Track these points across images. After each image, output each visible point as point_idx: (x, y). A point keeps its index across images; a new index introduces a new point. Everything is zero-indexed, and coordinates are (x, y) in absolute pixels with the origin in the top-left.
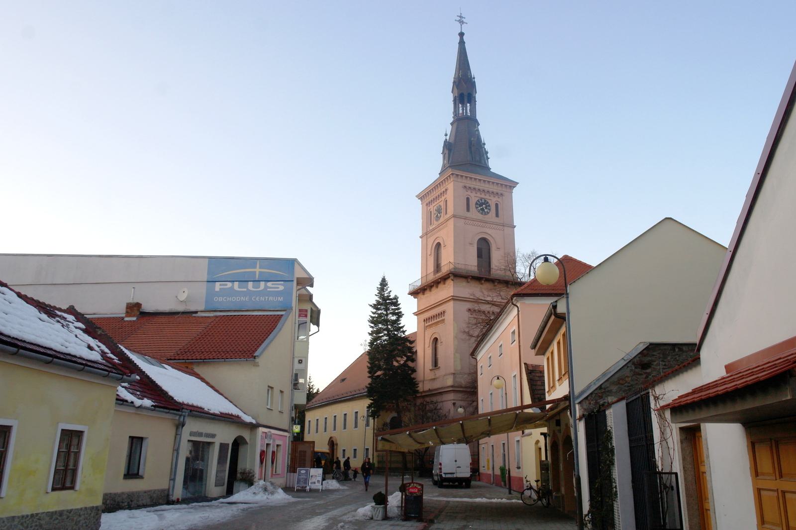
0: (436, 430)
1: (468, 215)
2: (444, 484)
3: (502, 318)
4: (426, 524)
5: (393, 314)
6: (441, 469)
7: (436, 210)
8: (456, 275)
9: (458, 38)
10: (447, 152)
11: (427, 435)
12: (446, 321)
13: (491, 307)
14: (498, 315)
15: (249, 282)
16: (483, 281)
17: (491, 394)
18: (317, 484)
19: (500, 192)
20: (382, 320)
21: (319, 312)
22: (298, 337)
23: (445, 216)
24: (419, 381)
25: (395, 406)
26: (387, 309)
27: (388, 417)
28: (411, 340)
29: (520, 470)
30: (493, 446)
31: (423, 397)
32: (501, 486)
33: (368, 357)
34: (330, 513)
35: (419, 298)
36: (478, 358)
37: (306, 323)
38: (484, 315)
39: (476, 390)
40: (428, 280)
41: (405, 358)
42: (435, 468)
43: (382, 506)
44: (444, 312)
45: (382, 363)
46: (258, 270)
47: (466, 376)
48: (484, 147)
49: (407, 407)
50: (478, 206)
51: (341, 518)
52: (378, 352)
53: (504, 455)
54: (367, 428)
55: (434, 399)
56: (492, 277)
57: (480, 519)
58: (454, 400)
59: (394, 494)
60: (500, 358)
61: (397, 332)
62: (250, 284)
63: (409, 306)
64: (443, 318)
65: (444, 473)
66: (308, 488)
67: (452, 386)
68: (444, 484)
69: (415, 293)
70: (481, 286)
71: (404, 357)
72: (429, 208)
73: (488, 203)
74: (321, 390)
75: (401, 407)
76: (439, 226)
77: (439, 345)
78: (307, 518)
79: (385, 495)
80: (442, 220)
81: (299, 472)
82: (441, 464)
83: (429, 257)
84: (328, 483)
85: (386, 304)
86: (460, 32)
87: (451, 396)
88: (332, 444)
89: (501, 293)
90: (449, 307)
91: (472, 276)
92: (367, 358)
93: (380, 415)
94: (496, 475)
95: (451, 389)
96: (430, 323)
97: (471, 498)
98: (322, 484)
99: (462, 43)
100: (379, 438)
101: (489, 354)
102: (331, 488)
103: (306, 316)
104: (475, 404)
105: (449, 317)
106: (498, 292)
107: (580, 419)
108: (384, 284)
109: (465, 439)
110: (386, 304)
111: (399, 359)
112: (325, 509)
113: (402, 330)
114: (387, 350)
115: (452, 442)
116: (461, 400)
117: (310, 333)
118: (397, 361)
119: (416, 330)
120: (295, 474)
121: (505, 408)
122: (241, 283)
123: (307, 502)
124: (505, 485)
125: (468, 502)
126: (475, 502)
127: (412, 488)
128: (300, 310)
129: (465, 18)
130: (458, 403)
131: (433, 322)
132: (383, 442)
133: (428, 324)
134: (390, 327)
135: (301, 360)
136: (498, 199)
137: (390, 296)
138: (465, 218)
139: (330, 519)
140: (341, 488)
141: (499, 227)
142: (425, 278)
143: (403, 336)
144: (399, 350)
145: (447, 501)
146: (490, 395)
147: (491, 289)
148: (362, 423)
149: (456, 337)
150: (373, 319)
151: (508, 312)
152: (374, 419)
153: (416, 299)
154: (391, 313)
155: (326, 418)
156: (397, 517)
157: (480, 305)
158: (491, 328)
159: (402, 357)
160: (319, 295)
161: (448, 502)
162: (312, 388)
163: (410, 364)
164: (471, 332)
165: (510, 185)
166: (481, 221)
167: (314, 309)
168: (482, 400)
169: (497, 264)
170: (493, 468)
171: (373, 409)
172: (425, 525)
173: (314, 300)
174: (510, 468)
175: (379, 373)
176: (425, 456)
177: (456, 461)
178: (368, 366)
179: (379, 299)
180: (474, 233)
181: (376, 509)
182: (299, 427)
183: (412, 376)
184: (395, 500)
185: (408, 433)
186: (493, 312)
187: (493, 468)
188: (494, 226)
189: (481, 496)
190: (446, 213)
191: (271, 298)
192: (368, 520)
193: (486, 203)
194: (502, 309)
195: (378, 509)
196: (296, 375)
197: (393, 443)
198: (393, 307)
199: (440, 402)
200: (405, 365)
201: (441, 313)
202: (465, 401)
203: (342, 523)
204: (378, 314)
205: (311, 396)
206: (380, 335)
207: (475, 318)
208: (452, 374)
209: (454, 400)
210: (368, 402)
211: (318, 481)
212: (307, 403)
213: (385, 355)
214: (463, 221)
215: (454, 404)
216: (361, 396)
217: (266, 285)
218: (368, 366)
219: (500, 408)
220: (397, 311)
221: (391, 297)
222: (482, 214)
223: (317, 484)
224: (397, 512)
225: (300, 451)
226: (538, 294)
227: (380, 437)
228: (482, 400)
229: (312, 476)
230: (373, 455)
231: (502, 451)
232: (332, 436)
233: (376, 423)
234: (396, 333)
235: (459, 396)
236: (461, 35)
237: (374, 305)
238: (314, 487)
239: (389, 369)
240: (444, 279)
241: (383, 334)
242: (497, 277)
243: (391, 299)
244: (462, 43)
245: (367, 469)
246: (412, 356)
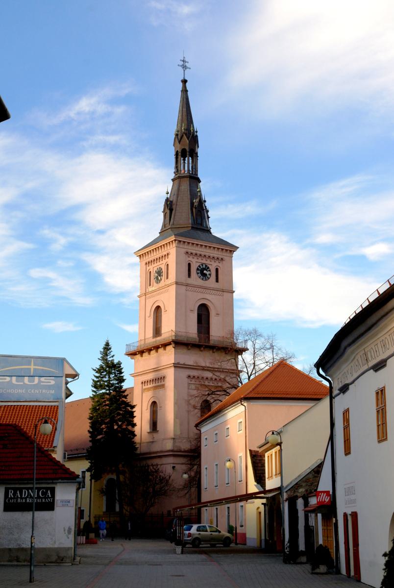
9: (181, 84)
10: (168, 212)
15: (25, 377)
19: (220, 257)
29: (243, 528)
46: (32, 367)
48: (205, 205)
55: (155, 461)
56: (212, 343)
58: (173, 463)
62: (26, 379)
63: (129, 367)
67: (172, 451)
73: (208, 268)
76: (159, 289)
80: (162, 284)
86: (182, 79)
87: (171, 460)
91: (192, 344)
95: (171, 453)
99: (185, 91)
107: (286, 501)
108: (107, 348)
116: (182, 464)
122: (18, 377)
129: (188, 62)
133: (146, 387)
136: (219, 264)
138: (187, 285)
141: (219, 292)
153: (133, 360)
163: (130, 428)
165: (231, 249)
166: (201, 287)
178: (89, 431)
180: (195, 299)
190: (167, 278)
191: (44, 391)
193: (207, 268)
208: (172, 438)
209: (173, 463)
214: (184, 287)
215: (174, 467)
217: (39, 380)
226: (261, 397)
228: (206, 468)
236: (184, 82)
242: (216, 344)
244: (185, 91)
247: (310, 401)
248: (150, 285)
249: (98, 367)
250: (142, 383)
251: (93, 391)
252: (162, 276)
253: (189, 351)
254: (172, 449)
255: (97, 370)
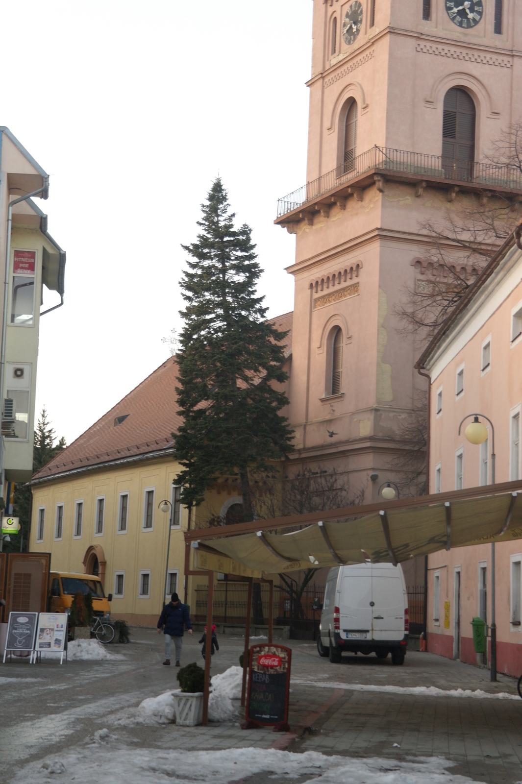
0: (323, 528)
1: (427, 27)
2: (344, 654)
3: (494, 279)
4: (294, 736)
5: (239, 268)
6: (337, 620)
7: (347, 16)
8: (389, 178)
11: (304, 543)
12: (361, 288)
13: (468, 257)
14: (483, 276)
16: (454, 195)
17: (460, 456)
18: (54, 648)
20: (213, 281)
21: (61, 258)
22: (13, 317)
23: (369, 30)
24: (295, 427)
25: (239, 481)
26: (223, 258)
27: (221, 504)
28: (280, 330)
30: (459, 573)
31: (303, 461)
32: (474, 663)
33: (177, 367)
34: (78, 710)
35: (300, 233)
36: (434, 375)
37: (32, 283)
38: (451, 275)
39: (424, 449)
40: (322, 191)
41: (264, 373)
42: (324, 618)
43: (197, 694)
44: (358, 265)
45: (210, 383)
47: (403, 416)
49: (265, 483)
50: (452, 4)
51: (105, 719)
52: (203, 357)
53: (485, 594)
54: (173, 527)
55: (329, 466)
56: (475, 184)
57: (419, 731)
58: (373, 469)
59: (228, 672)
60: (483, 374)
61: (247, 310)
63: (276, 253)
64: (355, 280)
65: (345, 631)
66: (33, 657)
67: (370, 439)
68: (344, 654)
69: (291, 221)
70: (449, 205)
71: (260, 368)
72: (330, 10)
74: (68, 443)
75: (251, 483)
77: (343, 343)
78: (26, 719)
79: (204, 671)
80: (361, 40)
81: (14, 620)
82: (337, 610)
83: (325, 132)
84: (79, 646)
85: (222, 246)
87: (368, 461)
88: (93, 561)
89: (497, 223)
90: (371, 256)
92: (176, 370)
93: (203, 500)
94: (464, 638)
95: (368, 444)
96: (326, 292)
97: (402, 686)
98: (66, 648)
100: (194, 544)
101: (457, 365)
102: (85, 657)
103: (32, 267)
104: (422, 478)
105: (370, 278)
106: (489, 221)
108: (217, 195)
109: (391, 553)
110: (222, 247)
111: (249, 373)
112: (70, 699)
113: (257, 306)
114: (223, 351)
115: (361, 559)
116: (391, 471)
117: (43, 309)
118: (246, 379)
119: (292, 309)
120: (5, 624)
121: (489, 483)
123: (27, 686)
124: (484, 661)
125: (395, 694)
126: (411, 695)
127: (266, 656)
128: (17, 254)
130: (383, 477)
131: (332, 289)
132: (203, 553)
133: (320, 294)
134: (230, 299)
135: (22, 370)
137: (231, 226)
139: (78, 721)
140: (109, 657)
141: (500, 58)
142: (316, 184)
143: (261, 320)
144: (249, 353)
145: (346, 690)
146: (456, 458)
147: (472, 214)
148: (161, 516)
149: (382, 326)
150: (191, 280)
151: (507, 267)
152: (189, 508)
153: (294, 236)
154: (233, 267)
155: (80, 505)
156: (230, 720)
157: (442, 252)
158: (466, 305)
159: (256, 370)
160: (63, 216)
161: (351, 692)
162: (49, 436)
163: (275, 385)
164: (420, 315)
166: (456, 44)
167: (50, 251)
168: (439, 470)
169: (490, 153)
170: (458, 623)
171: (187, 485)
172: (294, 739)
173: (51, 230)
174: (497, 623)
175: (203, 405)
176: (304, 594)
177: (372, 604)
178: (177, 389)
179: (205, 233)
180: (439, 73)
181: (183, 702)
182: (15, 521)
183: (280, 413)
184: (227, 683)
185: (259, 534)
186: (474, 270)
187: (458, 623)
188: (489, 56)
189: (427, 682)
190: (372, 24)
192: (164, 724)
194: (494, 260)
195: (187, 700)
196: (9, 403)
197: (226, 556)
198: (239, 254)
199: (341, 474)
200: (263, 387)
201: (352, 268)
202: (399, 471)
203: (105, 730)
204: (202, 268)
205: (44, 453)
206: (208, 317)
207: (430, 282)
209: (373, 469)
210: (176, 469)
211: (57, 641)
212: (35, 470)
213: (218, 364)
214: (412, 43)
215: (374, 478)
216: (161, 457)
218: (177, 389)
219: (480, 483)
220: (247, 263)
221: (235, 229)
222: (460, 25)
223: (54, 648)
224: (231, 708)
225: (16, 574)
227: (196, 542)
229: (42, 630)
230: (186, 588)
231: (480, 586)
232: (94, 543)
233: (194, 518)
234: (243, 313)
235: (385, 461)
237: (195, 246)
238: (46, 653)
239: (227, 400)
240: (361, 187)
241: (213, 316)
242: (489, 184)
243: (234, 234)
245: (174, 619)
246: (280, 368)
247: (50, 485)
248: (334, 51)
249: (196, 241)
250: (311, 285)
251: (188, 298)
252: (361, 22)
253: (419, 200)
254: (372, 434)
255: (191, 248)
